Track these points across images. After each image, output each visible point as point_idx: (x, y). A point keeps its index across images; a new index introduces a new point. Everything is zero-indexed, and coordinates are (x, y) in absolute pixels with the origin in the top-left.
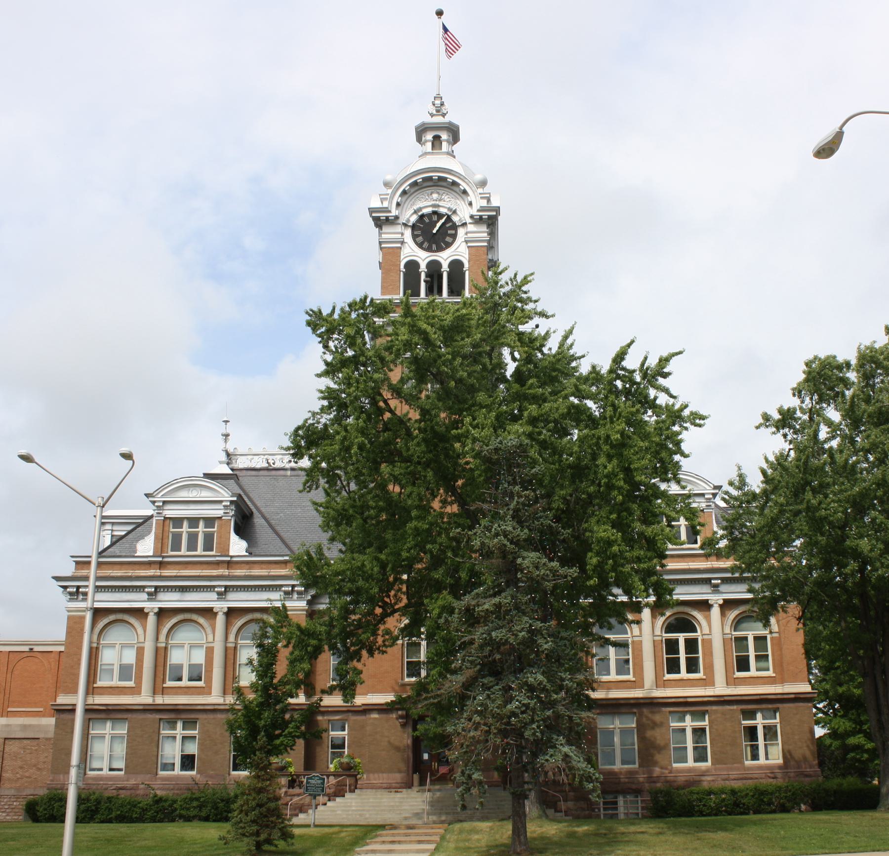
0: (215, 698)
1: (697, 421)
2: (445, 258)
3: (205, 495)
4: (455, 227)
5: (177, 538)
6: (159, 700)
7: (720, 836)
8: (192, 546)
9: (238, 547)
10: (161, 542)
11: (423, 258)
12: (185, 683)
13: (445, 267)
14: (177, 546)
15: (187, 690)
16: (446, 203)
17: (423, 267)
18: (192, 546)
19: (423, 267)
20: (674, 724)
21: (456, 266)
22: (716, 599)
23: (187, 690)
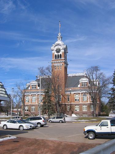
0: (36, 104)
1: (64, 110)
2: (59, 54)
3: (35, 83)
4: (60, 50)
5: (32, 87)
6: (31, 104)
7: (37, 58)
8: (34, 88)
9: (38, 88)
10: (31, 88)
11: (57, 54)
12: (77, 101)
13: (59, 55)
14: (32, 88)
15: (85, 102)
16: (59, 47)
17: (57, 55)
18: (34, 88)
19: (57, 55)
20: (83, 106)
21: (61, 55)
22: (37, 94)
23: (85, 102)
